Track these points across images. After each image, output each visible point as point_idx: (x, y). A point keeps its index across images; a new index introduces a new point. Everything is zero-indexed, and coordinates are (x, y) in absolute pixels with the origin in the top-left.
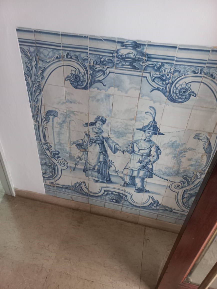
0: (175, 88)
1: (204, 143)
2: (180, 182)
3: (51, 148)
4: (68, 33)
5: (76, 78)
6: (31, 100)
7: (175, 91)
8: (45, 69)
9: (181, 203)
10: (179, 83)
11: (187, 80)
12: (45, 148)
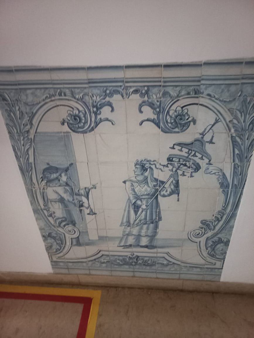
0: (168, 117)
1: (218, 176)
2: (200, 229)
3: (55, 215)
4: (40, 66)
5: (75, 119)
6: (21, 157)
7: (169, 121)
8: (33, 114)
9: (205, 254)
10: (172, 108)
11: (183, 102)
12: (46, 214)
